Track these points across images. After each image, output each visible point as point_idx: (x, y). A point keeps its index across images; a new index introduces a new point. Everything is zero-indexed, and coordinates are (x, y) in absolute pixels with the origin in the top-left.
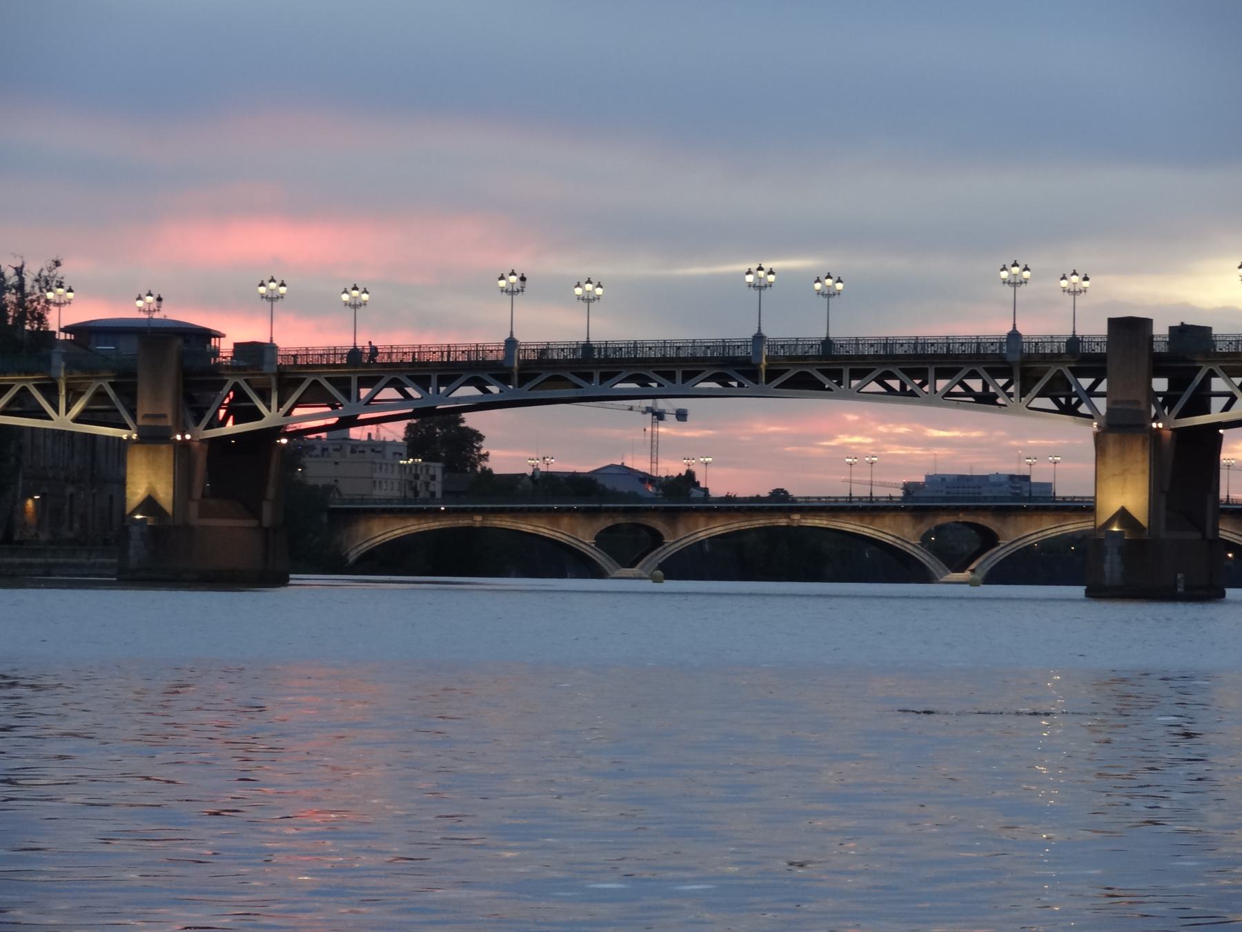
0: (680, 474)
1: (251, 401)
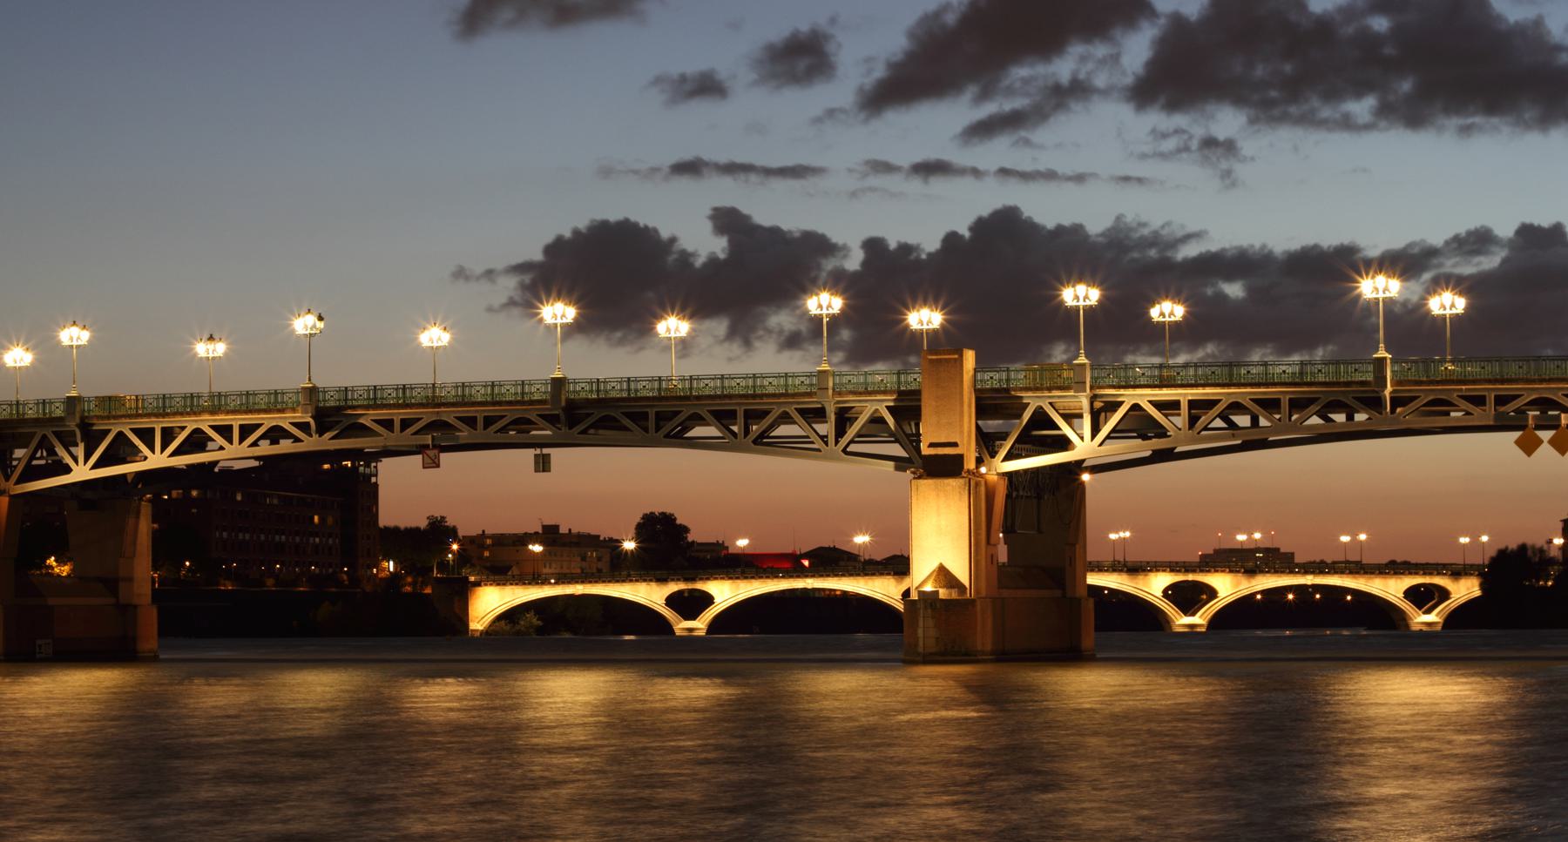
0: (599, 536)
1: (1058, 428)
